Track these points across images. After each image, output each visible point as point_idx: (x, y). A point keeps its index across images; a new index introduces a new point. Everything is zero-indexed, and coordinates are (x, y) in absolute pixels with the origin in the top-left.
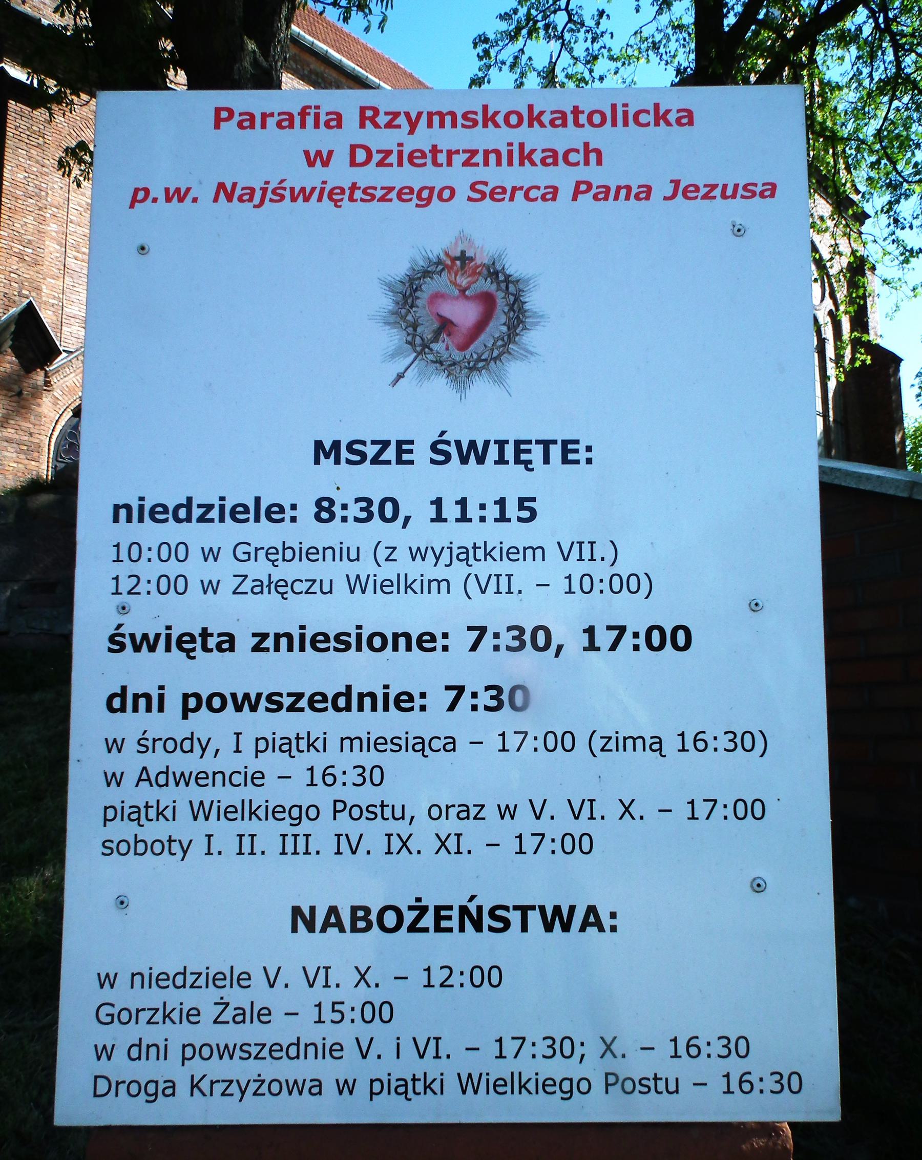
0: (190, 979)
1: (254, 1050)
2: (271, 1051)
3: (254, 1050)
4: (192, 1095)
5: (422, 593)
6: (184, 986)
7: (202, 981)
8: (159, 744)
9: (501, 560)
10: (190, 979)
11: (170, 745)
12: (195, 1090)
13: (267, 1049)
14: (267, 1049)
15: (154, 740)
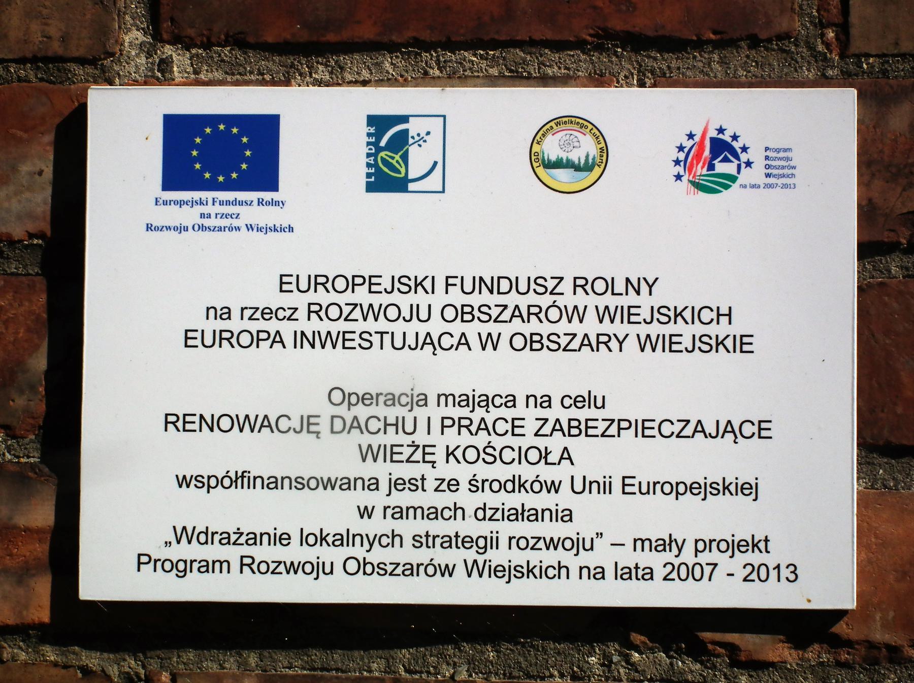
0: (489, 513)
1: (390, 568)
2: (449, 485)
3: (390, 568)
4: (447, 462)
5: (735, 351)
6: (484, 519)
7: (498, 515)
8: (487, 484)
9: (693, 323)
10: (489, 513)
11: (496, 486)
12: (451, 457)
13: (446, 483)
14: (446, 483)
15: (483, 481)
